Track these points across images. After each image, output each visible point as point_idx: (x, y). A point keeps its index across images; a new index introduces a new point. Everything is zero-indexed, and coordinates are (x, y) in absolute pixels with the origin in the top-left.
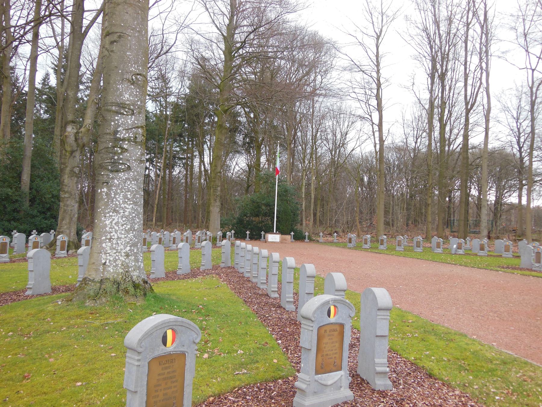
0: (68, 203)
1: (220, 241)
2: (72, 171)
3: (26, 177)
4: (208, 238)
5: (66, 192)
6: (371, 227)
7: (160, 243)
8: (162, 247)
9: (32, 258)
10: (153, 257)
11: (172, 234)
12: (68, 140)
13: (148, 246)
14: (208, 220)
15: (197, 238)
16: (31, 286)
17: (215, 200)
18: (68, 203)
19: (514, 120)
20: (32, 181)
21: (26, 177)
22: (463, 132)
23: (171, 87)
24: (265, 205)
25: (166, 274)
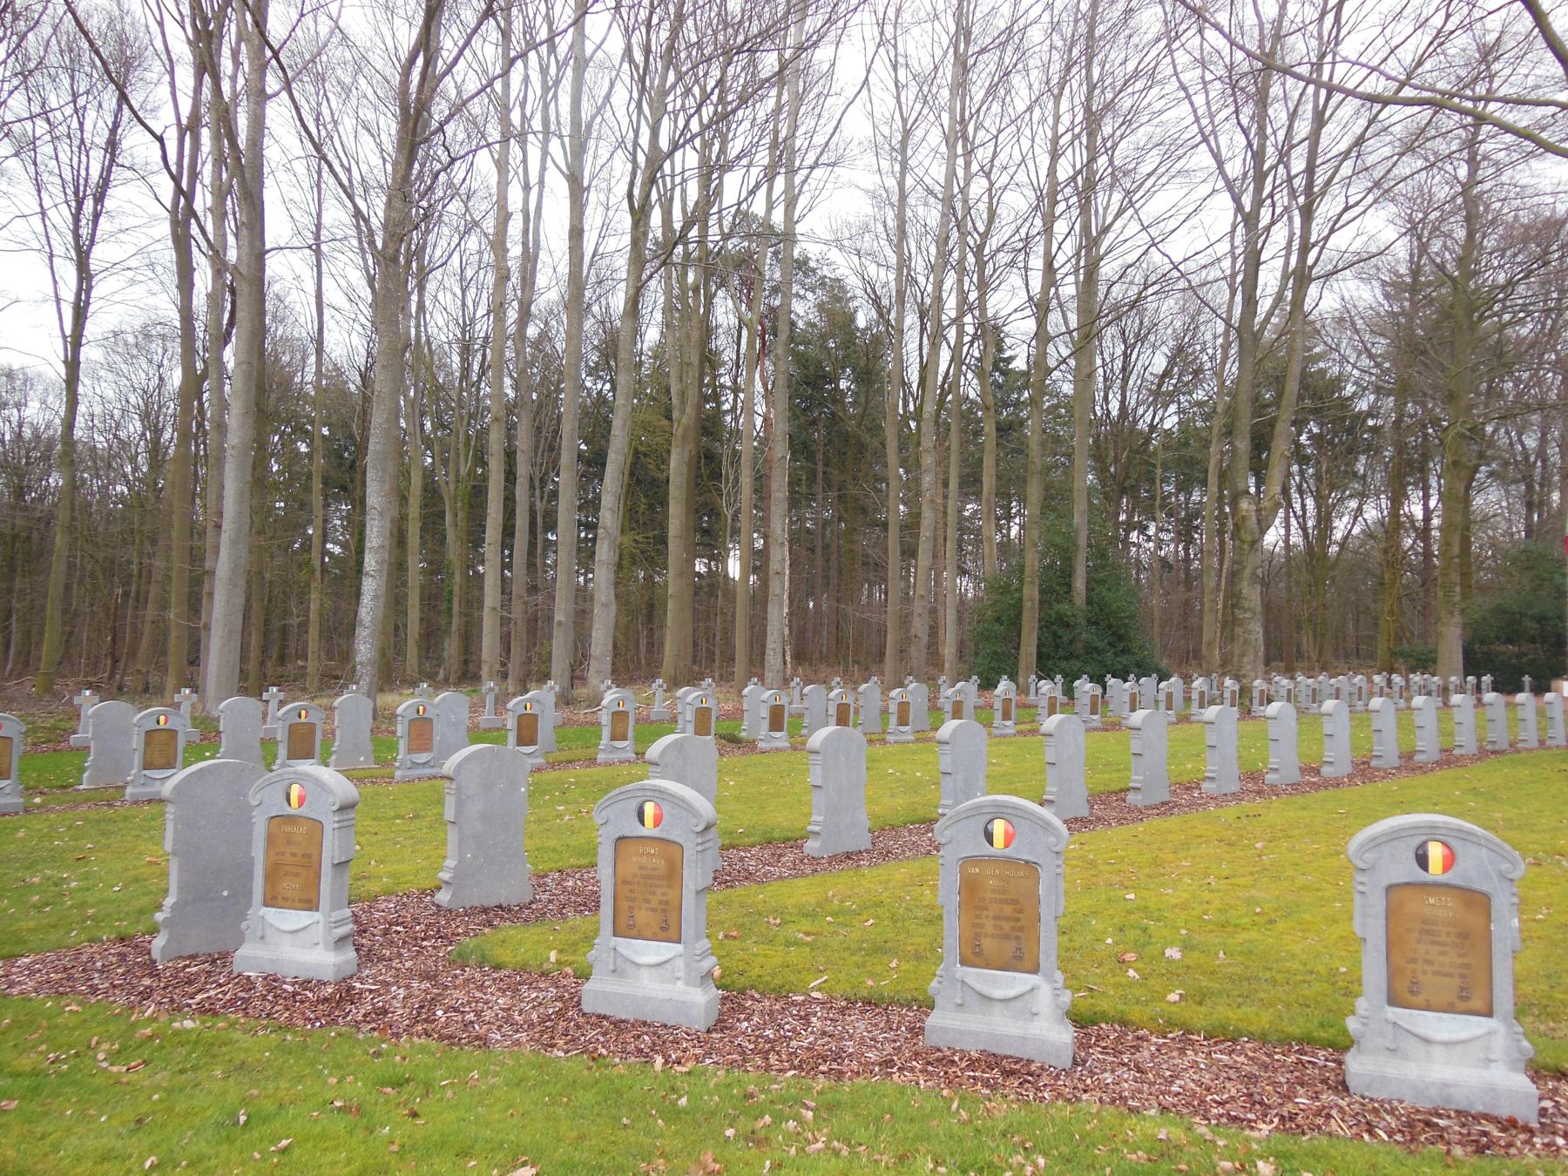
0: (1251, 627)
1: (1261, 704)
2: (1254, 574)
3: (1080, 584)
4: (1227, 695)
5: (1246, 610)
6: (1227, 666)
7: (1289, 700)
8: (1290, 708)
9: (451, 779)
10: (1419, 720)
11: (1333, 681)
12: (1247, 523)
13: (636, 740)
14: (194, 659)
15: (998, 705)
16: (817, 829)
17: (1451, 613)
18: (1251, 627)
19: (851, 23)
20: (1089, 589)
21: (1080, 584)
22: (1308, 300)
23: (1012, 359)
24: (1533, 617)
25: (1355, 765)
